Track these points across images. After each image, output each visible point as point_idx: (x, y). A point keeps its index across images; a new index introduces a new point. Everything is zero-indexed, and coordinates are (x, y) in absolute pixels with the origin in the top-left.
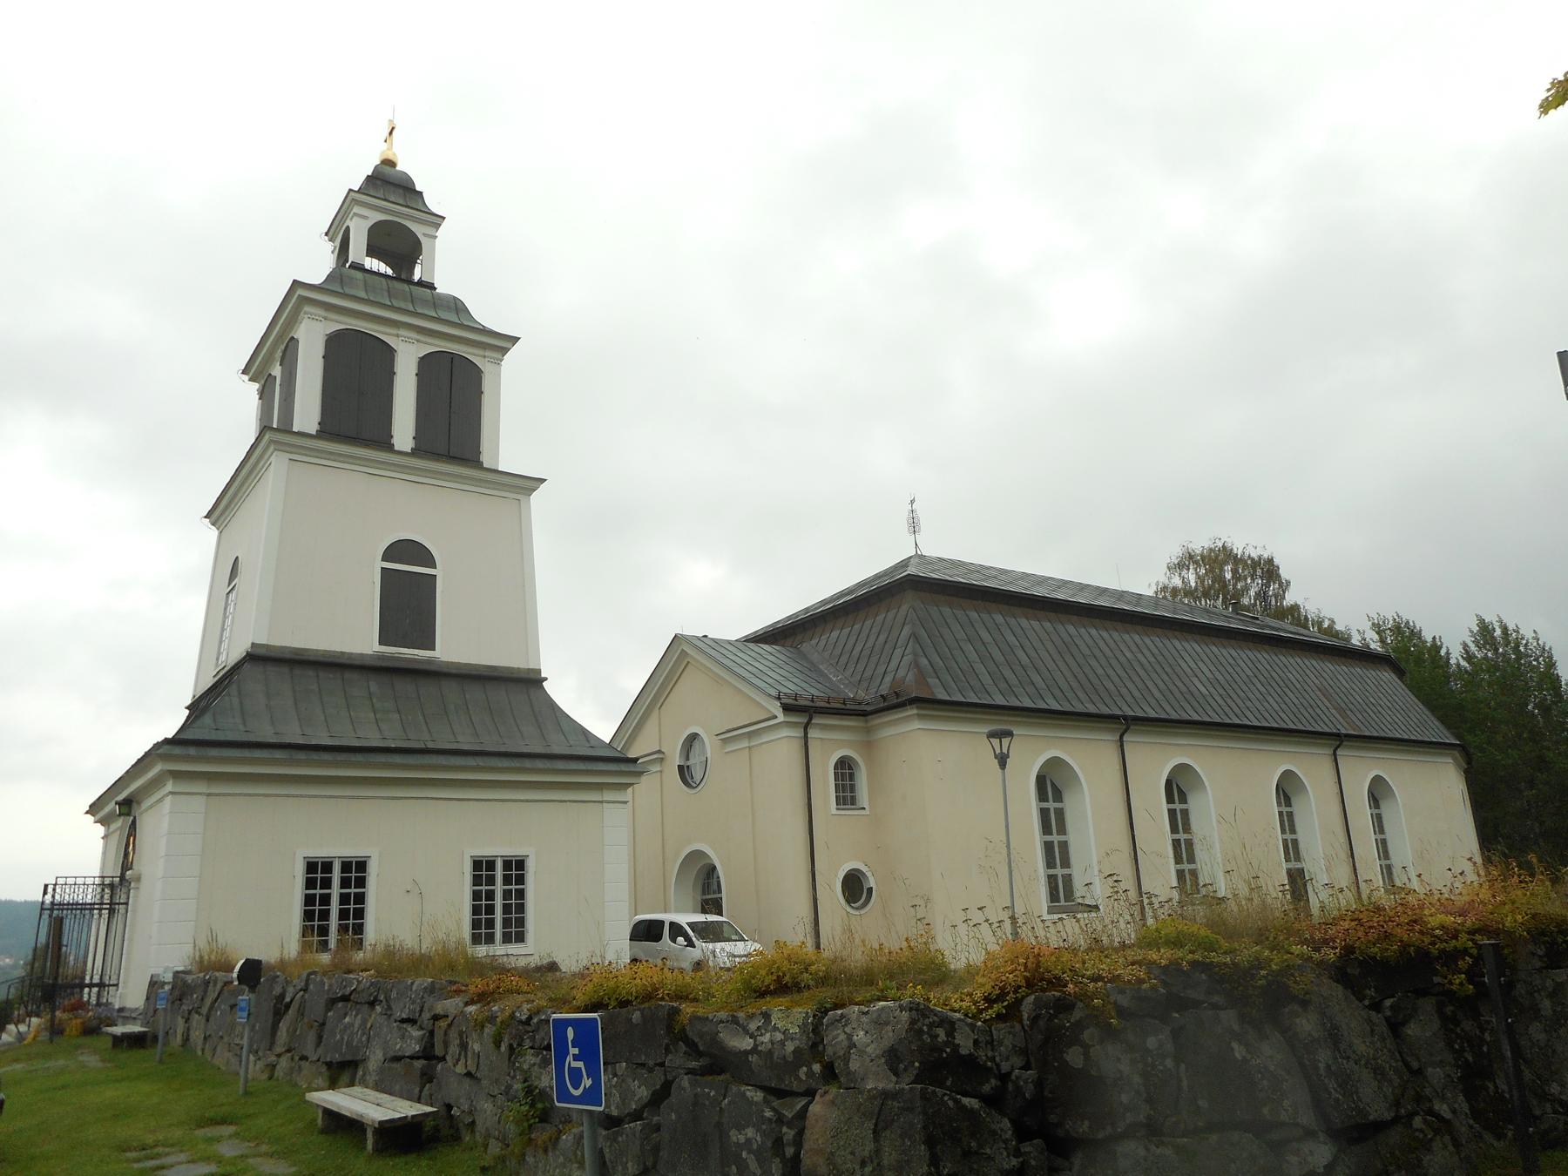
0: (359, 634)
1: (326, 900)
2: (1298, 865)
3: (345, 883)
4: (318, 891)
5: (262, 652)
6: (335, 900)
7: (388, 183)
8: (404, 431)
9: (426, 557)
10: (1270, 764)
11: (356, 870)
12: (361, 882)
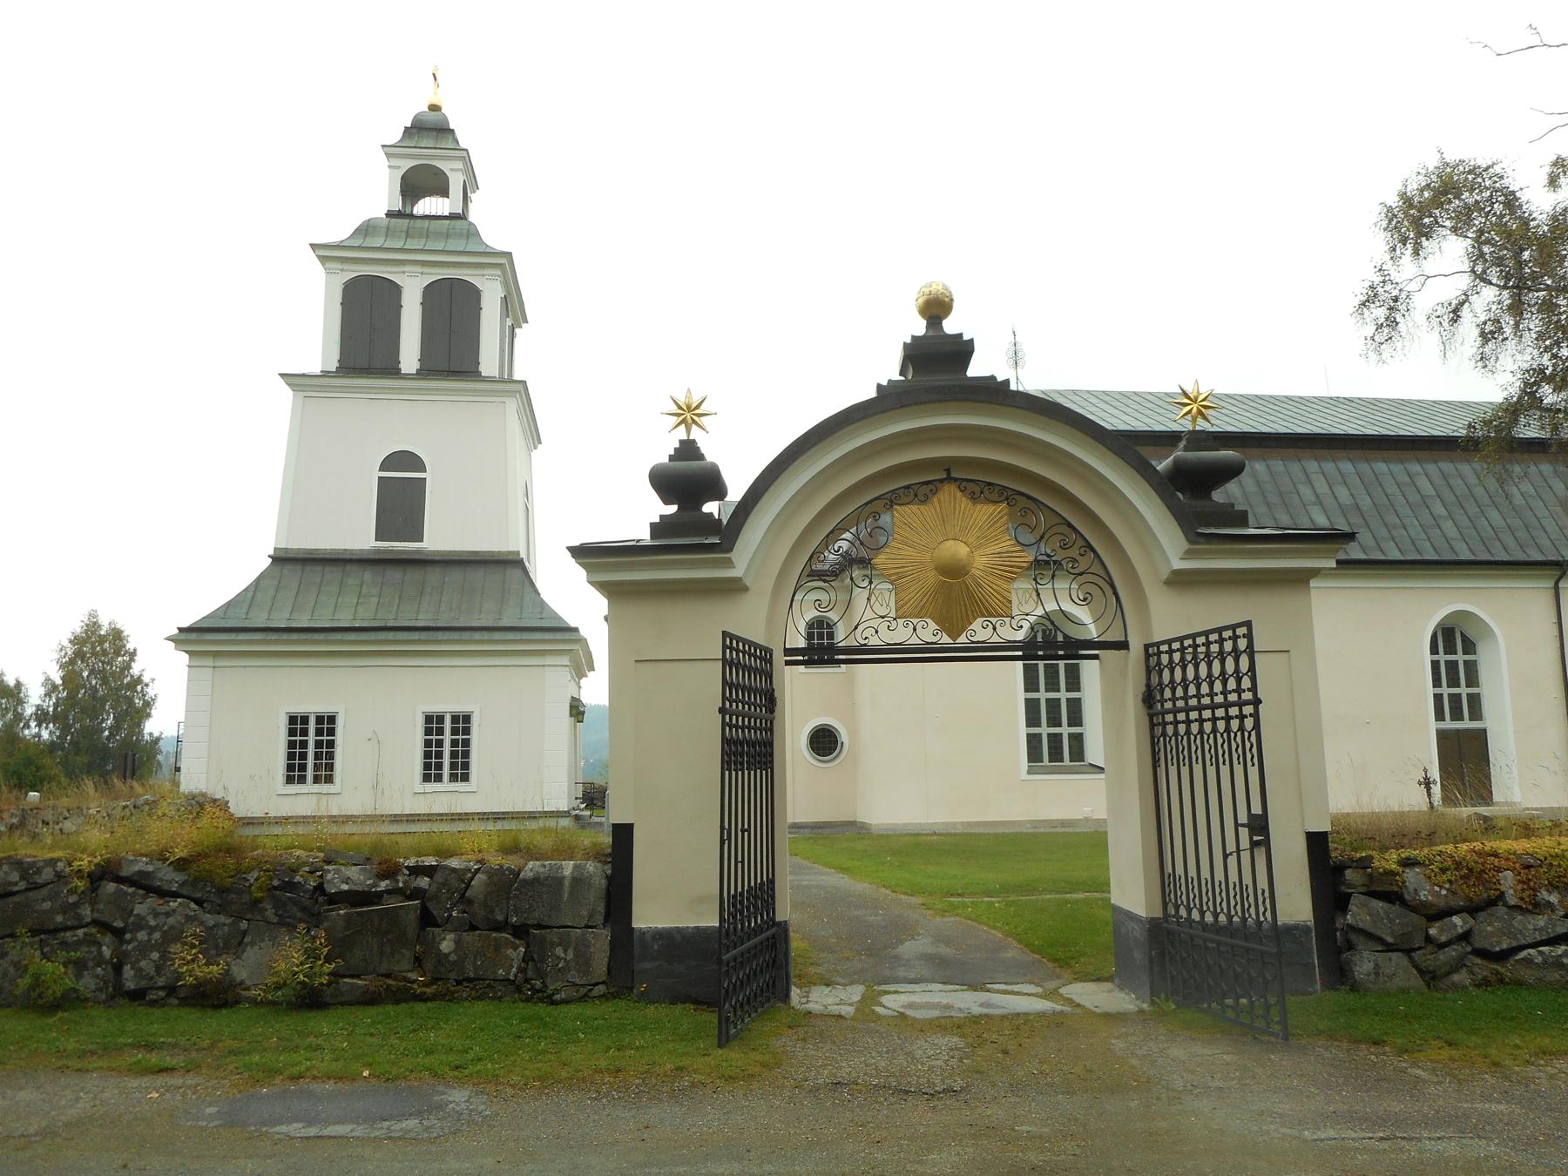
0: (361, 535)
1: (304, 744)
2: (1466, 724)
3: (319, 732)
4: (434, 737)
5: (282, 554)
6: (311, 745)
7: (430, 129)
8: (410, 356)
9: (419, 465)
10: (1425, 607)
11: (327, 723)
12: (332, 732)
